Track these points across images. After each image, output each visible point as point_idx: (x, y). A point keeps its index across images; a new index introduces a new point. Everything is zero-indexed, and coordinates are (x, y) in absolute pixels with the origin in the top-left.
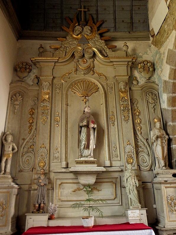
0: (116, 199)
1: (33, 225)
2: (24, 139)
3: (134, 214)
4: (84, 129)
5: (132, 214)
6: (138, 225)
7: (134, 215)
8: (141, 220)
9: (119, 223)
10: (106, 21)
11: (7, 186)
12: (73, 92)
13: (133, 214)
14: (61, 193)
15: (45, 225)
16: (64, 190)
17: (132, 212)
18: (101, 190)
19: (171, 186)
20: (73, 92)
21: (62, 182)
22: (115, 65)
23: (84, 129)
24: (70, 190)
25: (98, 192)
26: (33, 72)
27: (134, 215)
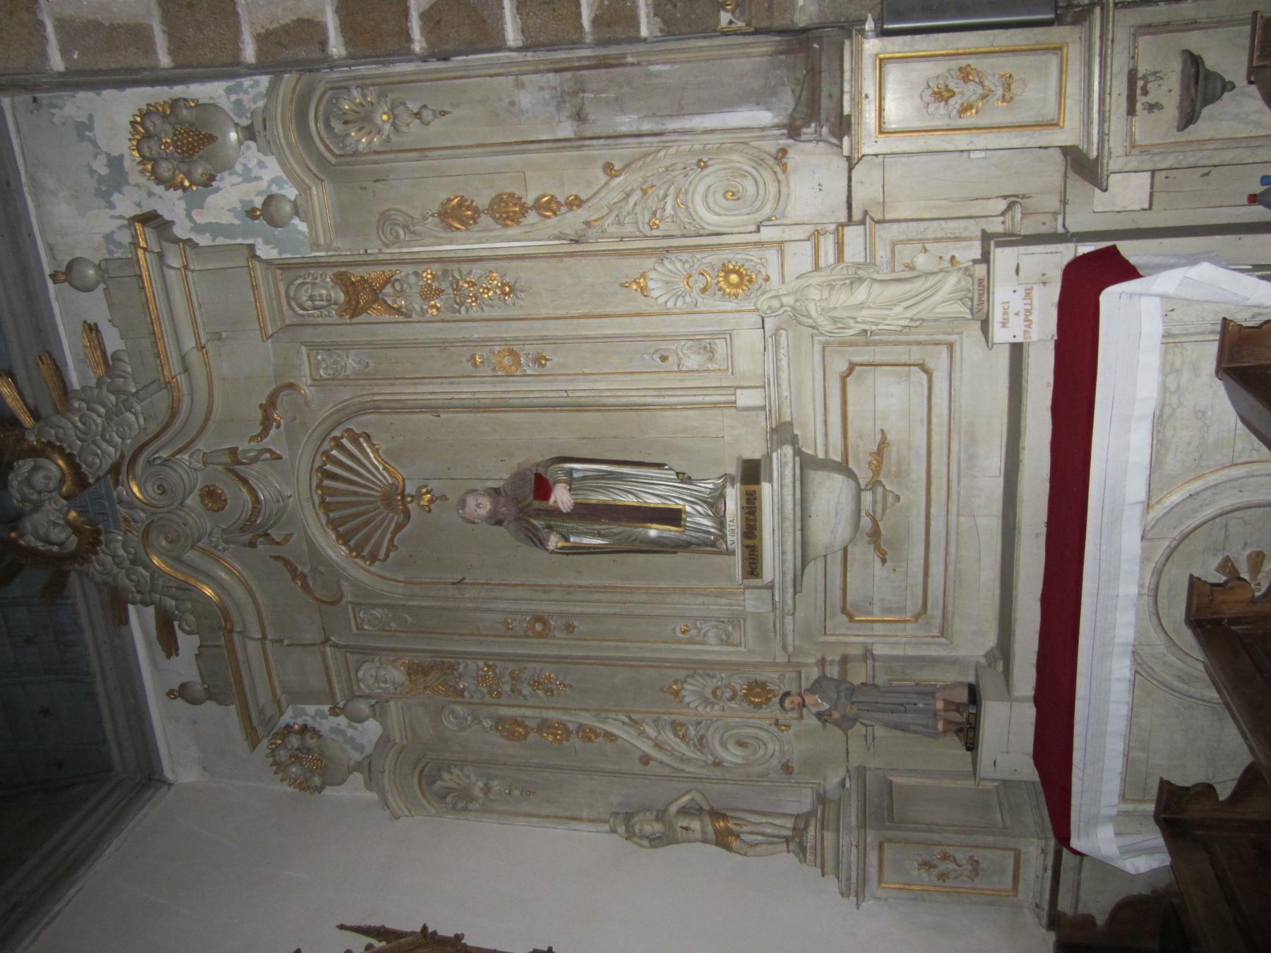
0: (931, 364)
1: (1025, 753)
2: (645, 759)
3: (1012, 312)
4: (806, 134)
5: (1010, 324)
6: (838, 74)
7: (1017, 314)
8: (1044, 279)
9: (1048, 384)
10: (85, 322)
11: (854, 850)
12: (387, 555)
13: (1012, 317)
14: (889, 611)
15: (1028, 713)
16: (877, 597)
17: (1004, 325)
18: (882, 431)
19: (872, 96)
20: (387, 555)
21: (838, 610)
22: (197, 337)
23: (806, 134)
24: (877, 572)
25: (894, 448)
26: (313, 718)
27: (1017, 314)
